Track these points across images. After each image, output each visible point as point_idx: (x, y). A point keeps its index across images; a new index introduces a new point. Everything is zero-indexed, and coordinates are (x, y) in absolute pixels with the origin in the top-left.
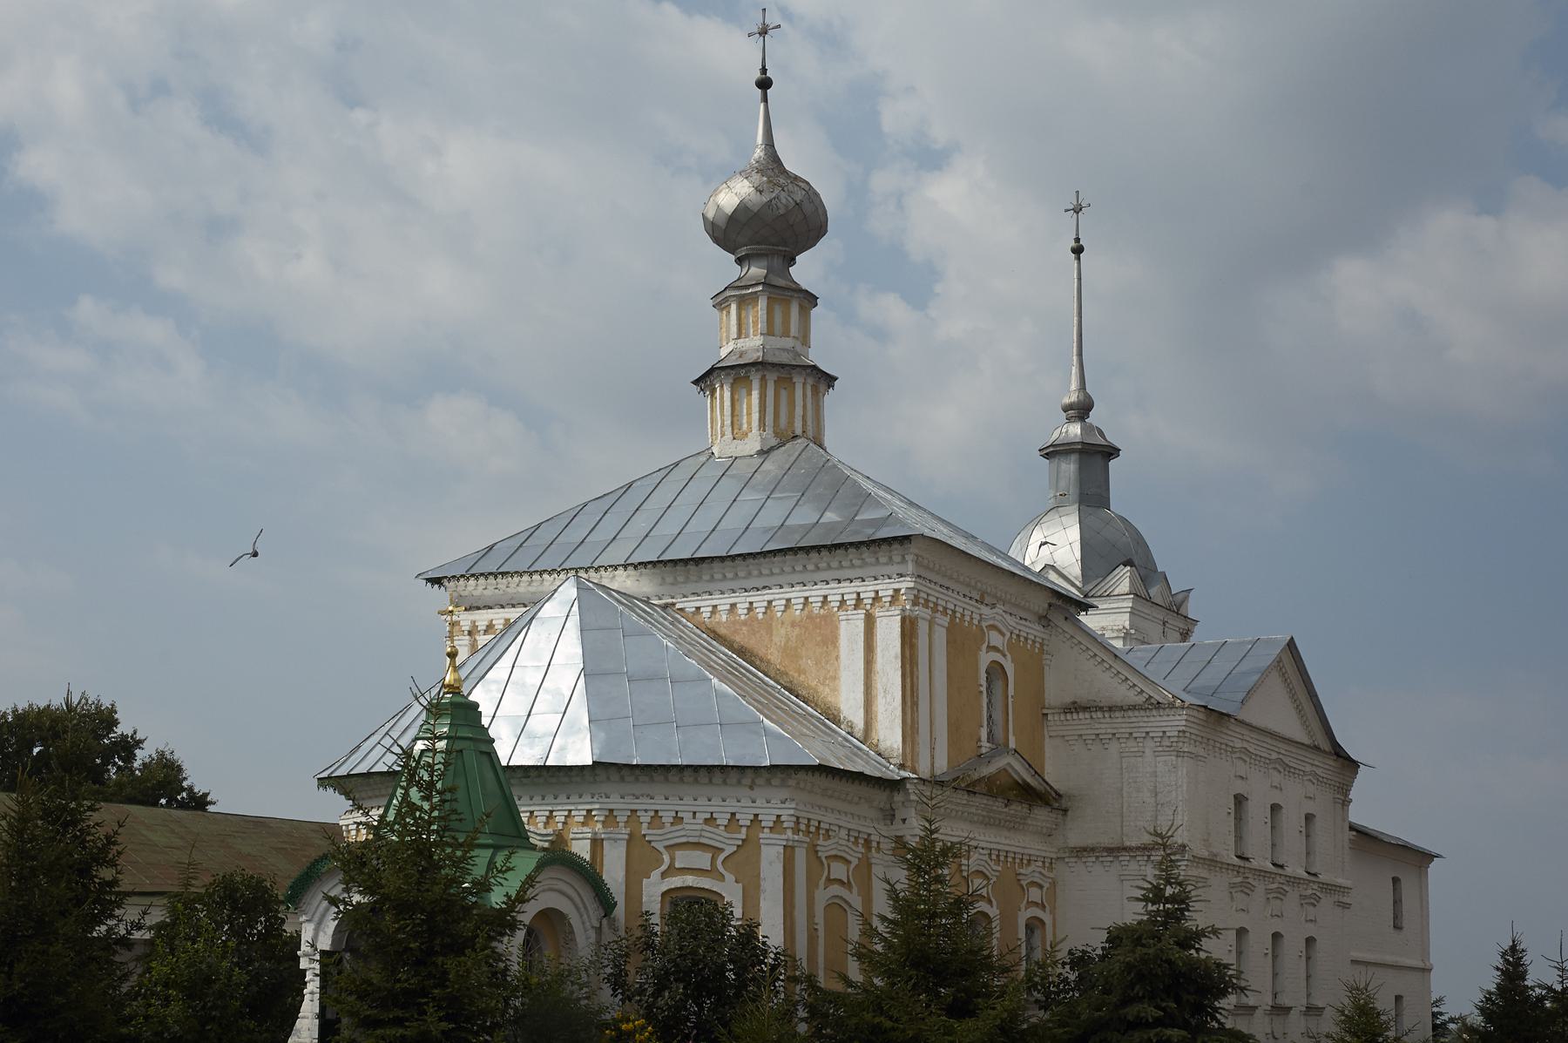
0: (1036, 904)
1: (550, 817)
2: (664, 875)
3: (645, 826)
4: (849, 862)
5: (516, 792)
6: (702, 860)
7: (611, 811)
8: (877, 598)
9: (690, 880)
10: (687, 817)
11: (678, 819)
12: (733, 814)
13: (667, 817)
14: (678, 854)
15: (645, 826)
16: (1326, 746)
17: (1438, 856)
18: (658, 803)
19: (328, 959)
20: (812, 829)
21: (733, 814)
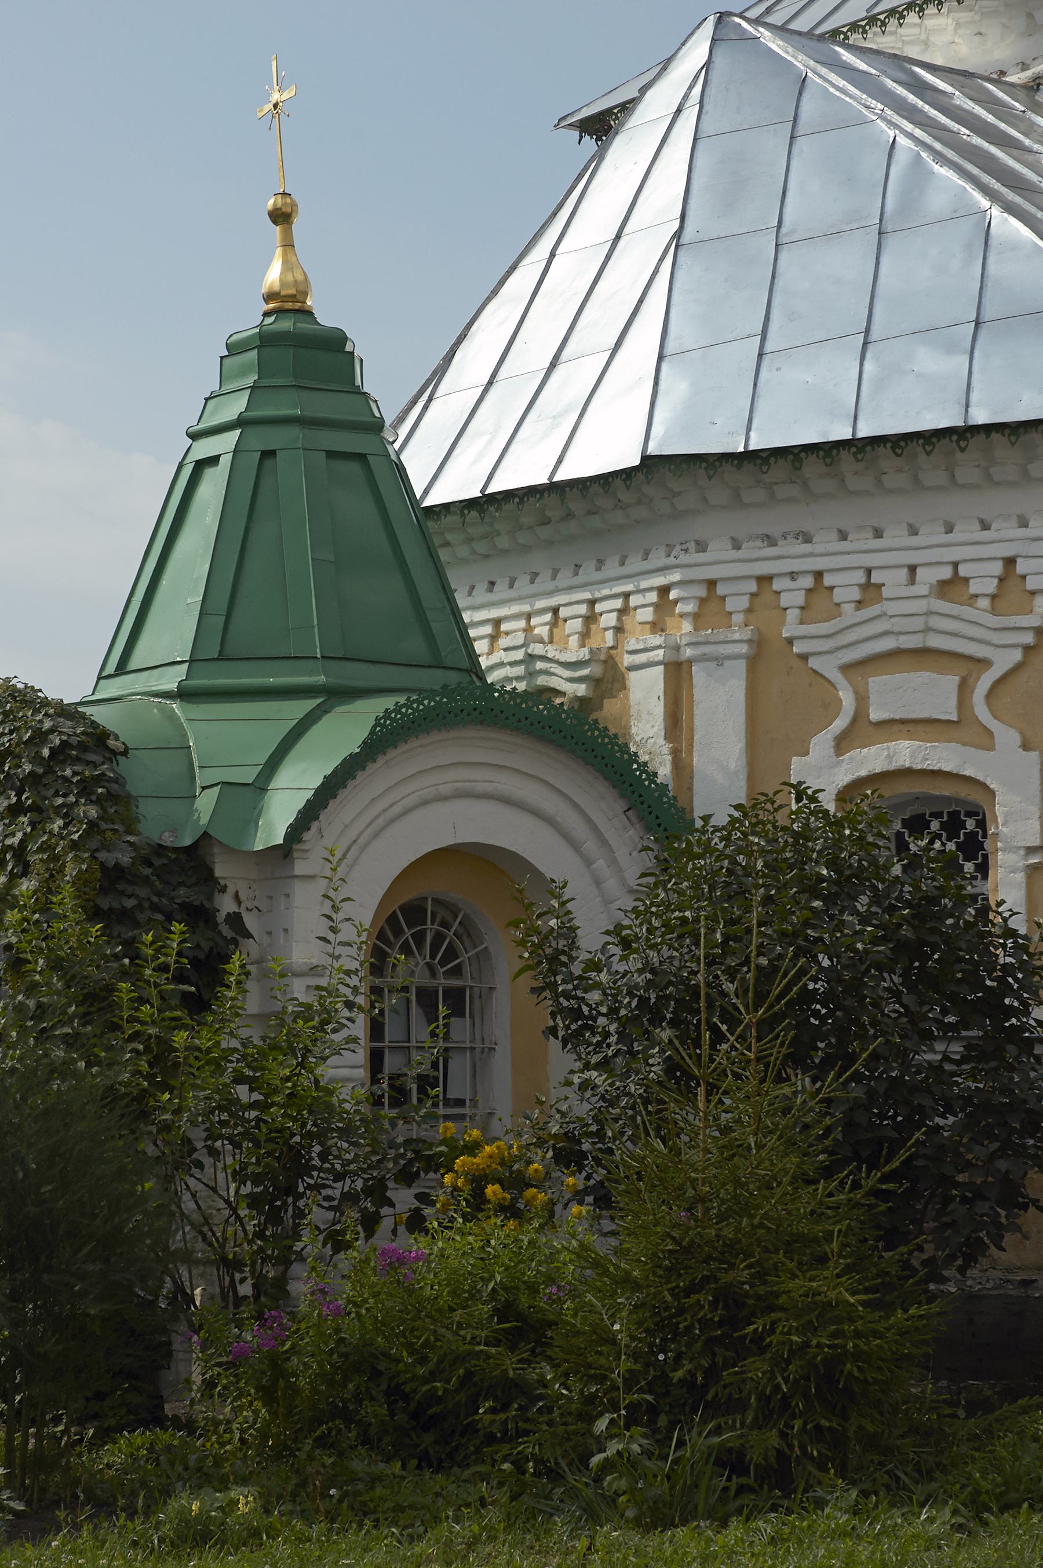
1: (590, 619)
2: (842, 743)
3: (793, 615)
5: (455, 578)
6: (932, 693)
7: (712, 584)
9: (905, 752)
10: (892, 581)
12: (1010, 562)
13: (846, 588)
14: (876, 683)
15: (793, 615)
17: (884, 585)
18: (824, 553)
21: (1010, 562)
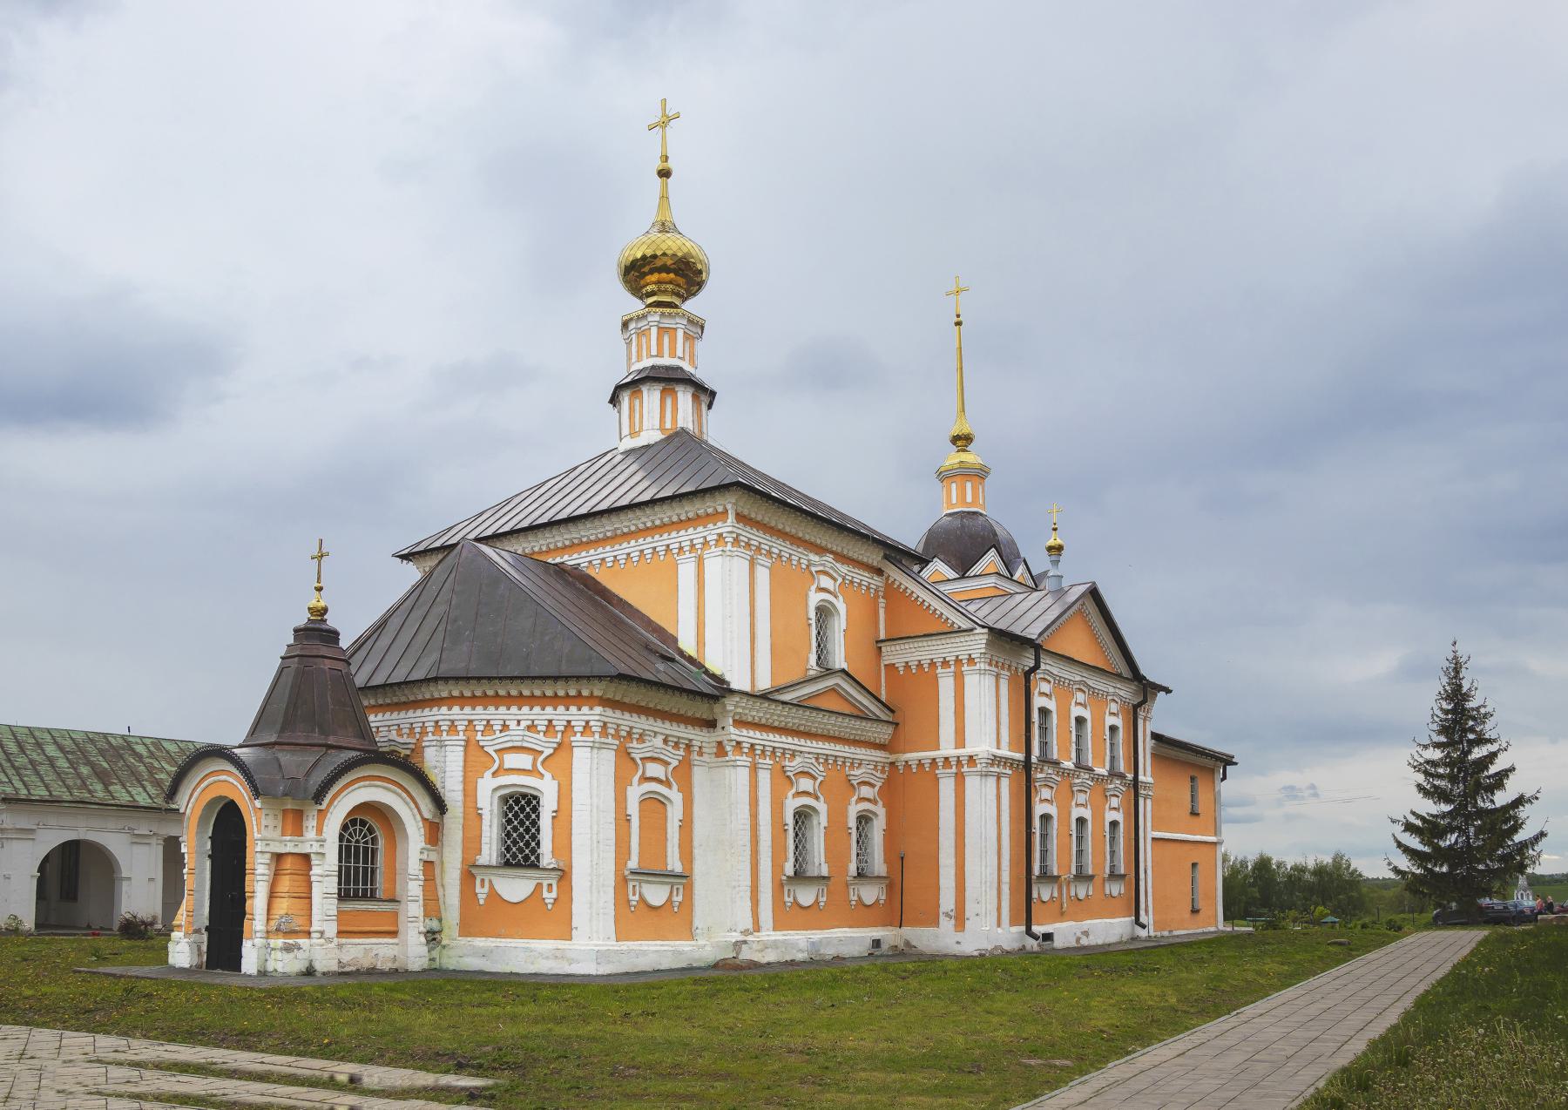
0: (868, 800)
2: (494, 774)
4: (667, 764)
6: (524, 761)
8: (706, 543)
10: (513, 725)
11: (505, 727)
16: (1126, 673)
19: (786, 860)
20: (623, 734)
